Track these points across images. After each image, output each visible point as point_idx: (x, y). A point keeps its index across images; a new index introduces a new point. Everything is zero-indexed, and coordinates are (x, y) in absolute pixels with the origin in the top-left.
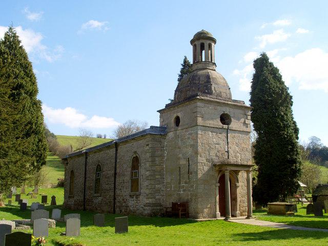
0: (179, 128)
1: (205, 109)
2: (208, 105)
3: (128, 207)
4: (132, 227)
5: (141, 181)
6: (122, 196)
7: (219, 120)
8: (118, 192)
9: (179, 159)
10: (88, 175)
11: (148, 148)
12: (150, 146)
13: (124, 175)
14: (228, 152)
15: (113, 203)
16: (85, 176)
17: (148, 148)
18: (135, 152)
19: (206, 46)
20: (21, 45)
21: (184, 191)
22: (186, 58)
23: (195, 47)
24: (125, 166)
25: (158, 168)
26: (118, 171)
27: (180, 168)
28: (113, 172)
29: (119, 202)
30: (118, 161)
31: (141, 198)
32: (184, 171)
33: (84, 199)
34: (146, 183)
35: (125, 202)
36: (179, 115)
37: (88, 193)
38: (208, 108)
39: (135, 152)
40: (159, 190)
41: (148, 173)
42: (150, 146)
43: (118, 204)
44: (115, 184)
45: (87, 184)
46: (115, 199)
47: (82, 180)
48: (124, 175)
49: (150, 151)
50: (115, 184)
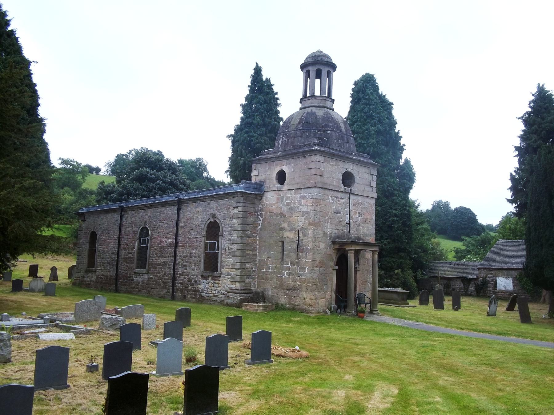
0: (285, 187)
1: (325, 164)
2: (328, 159)
3: (199, 291)
4: (87, 250)
5: (222, 257)
6: (188, 275)
7: (340, 176)
8: (180, 269)
9: (282, 229)
10: (123, 241)
11: (235, 211)
12: (240, 209)
13: (192, 246)
14: (348, 224)
15: (171, 284)
16: (119, 242)
17: (237, 212)
18: (214, 216)
19: (324, 74)
20: (10, 28)
21: (289, 274)
22: (258, 71)
23: (308, 74)
24: (194, 233)
25: (249, 240)
26: (181, 238)
27: (283, 242)
28: (172, 240)
29: (181, 283)
30: (181, 224)
31: (221, 280)
32: (290, 246)
33: (117, 275)
34: (231, 261)
35: (193, 285)
36: (285, 169)
37: (123, 266)
38: (329, 163)
39: (214, 216)
40: (250, 271)
41: (235, 247)
42: (240, 209)
43: (179, 286)
44: (175, 257)
45: (122, 254)
46: (174, 279)
47: (112, 246)
48: (192, 246)
49: (240, 216)
50: (175, 257)
